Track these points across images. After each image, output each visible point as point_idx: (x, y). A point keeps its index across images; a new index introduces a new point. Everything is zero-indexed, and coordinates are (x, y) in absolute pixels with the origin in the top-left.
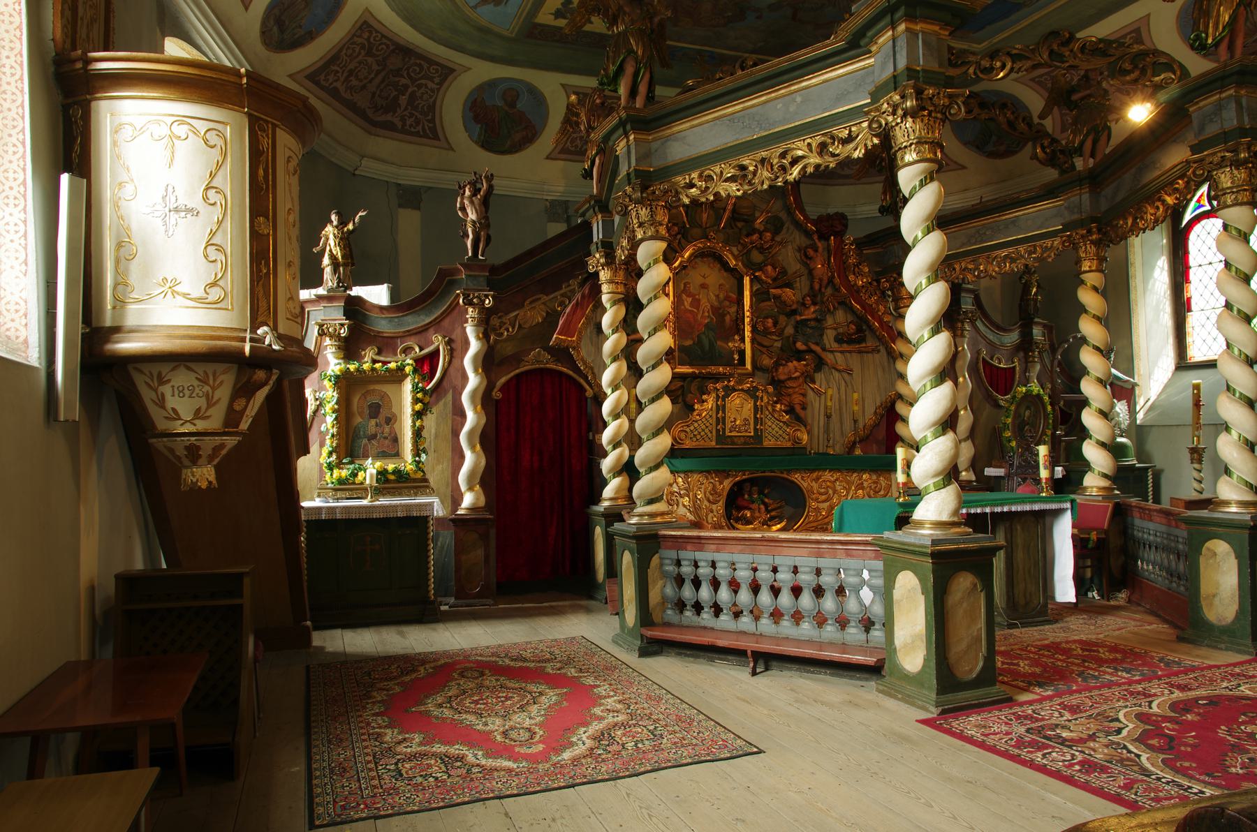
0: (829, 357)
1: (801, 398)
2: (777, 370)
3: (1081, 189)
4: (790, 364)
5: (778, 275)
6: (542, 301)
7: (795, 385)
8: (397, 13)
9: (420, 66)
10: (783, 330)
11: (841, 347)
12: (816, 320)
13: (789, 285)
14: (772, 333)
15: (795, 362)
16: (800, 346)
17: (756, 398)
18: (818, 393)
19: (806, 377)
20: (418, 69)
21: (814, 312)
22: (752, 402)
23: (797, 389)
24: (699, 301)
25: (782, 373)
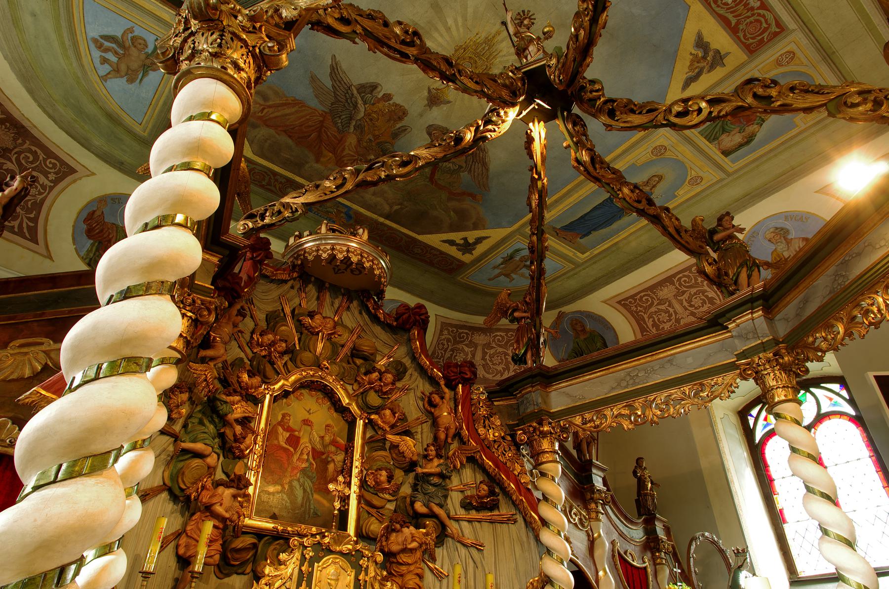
0: (453, 527)
1: (417, 580)
2: (387, 539)
3: (752, 313)
4: (405, 530)
5: (397, 422)
6: (43, 348)
7: (410, 561)
8: (10, 64)
9: (35, 154)
10: (398, 487)
11: (469, 514)
12: (441, 476)
13: (407, 433)
14: (384, 490)
15: (412, 528)
16: (419, 507)
17: (358, 569)
18: (439, 576)
19: (424, 552)
20: (31, 159)
21: (438, 466)
22: (353, 574)
23: (412, 568)
24: (298, 438)
25: (395, 542)
